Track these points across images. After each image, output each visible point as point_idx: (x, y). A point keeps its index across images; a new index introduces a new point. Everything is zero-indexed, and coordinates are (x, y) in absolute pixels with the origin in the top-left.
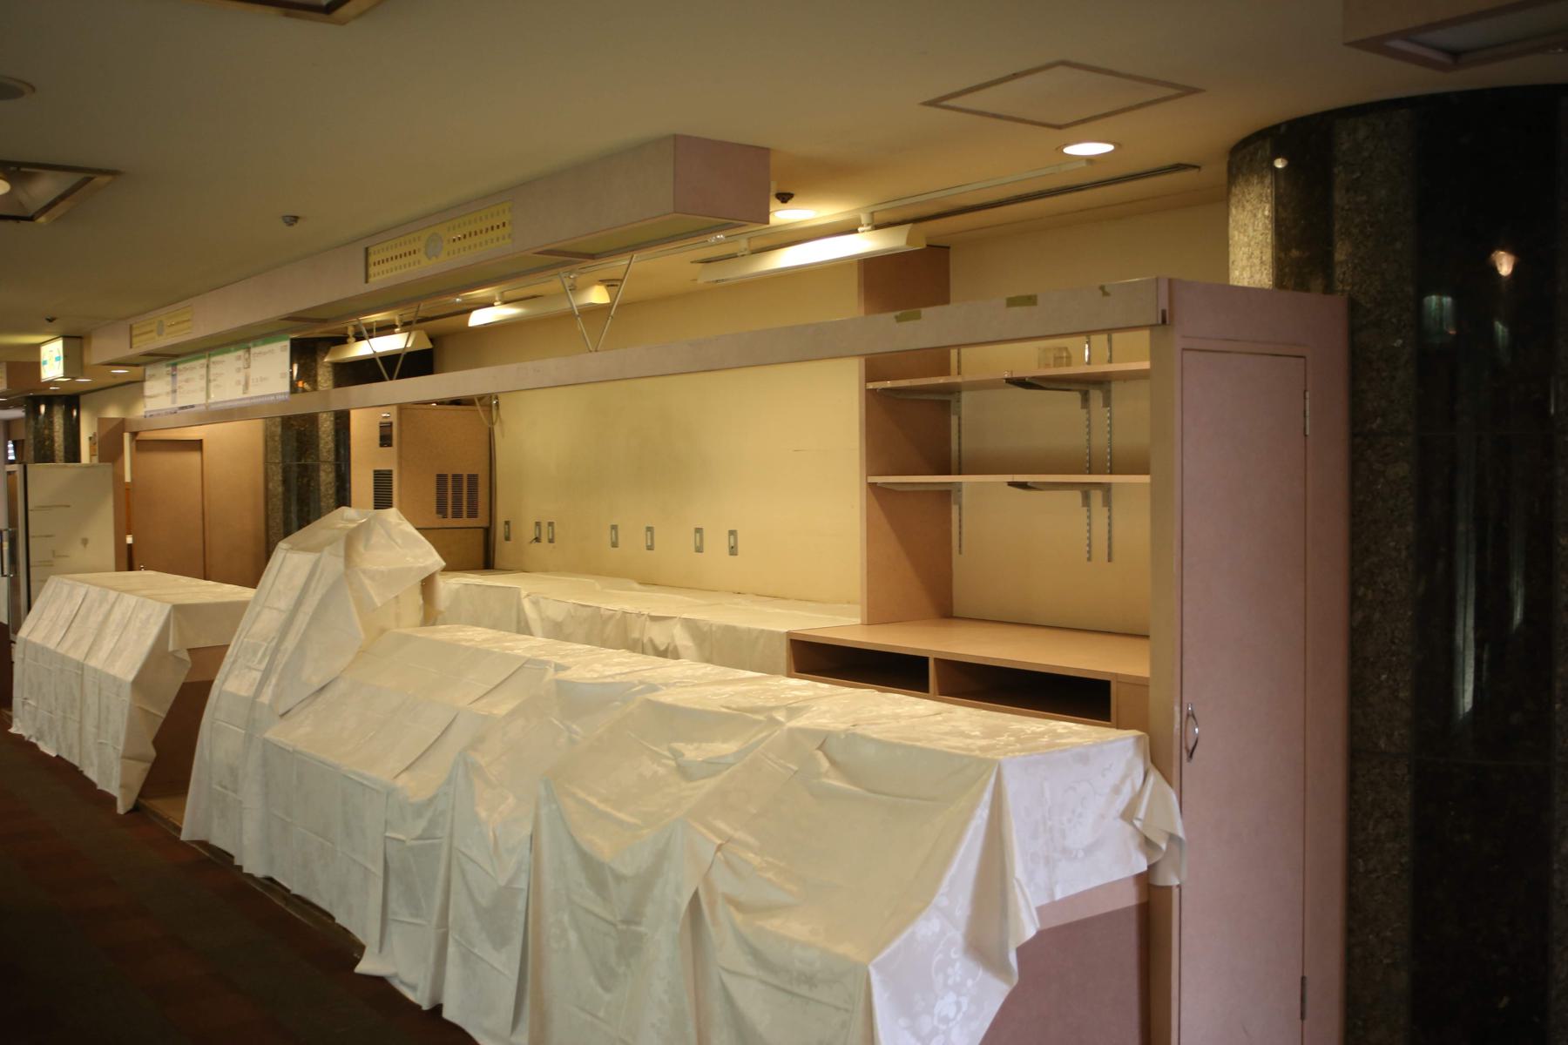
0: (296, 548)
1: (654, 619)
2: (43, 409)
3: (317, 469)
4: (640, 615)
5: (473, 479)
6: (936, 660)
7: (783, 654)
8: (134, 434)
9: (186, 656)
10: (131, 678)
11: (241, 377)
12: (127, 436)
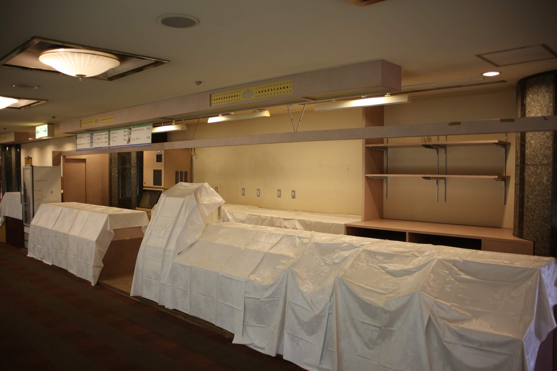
0: (168, 196)
1: (285, 219)
2: (7, 149)
3: (130, 169)
4: (279, 218)
5: (186, 173)
6: (409, 233)
7: (343, 230)
8: (64, 157)
9: (112, 232)
10: (95, 239)
11: (127, 138)
12: (62, 157)
